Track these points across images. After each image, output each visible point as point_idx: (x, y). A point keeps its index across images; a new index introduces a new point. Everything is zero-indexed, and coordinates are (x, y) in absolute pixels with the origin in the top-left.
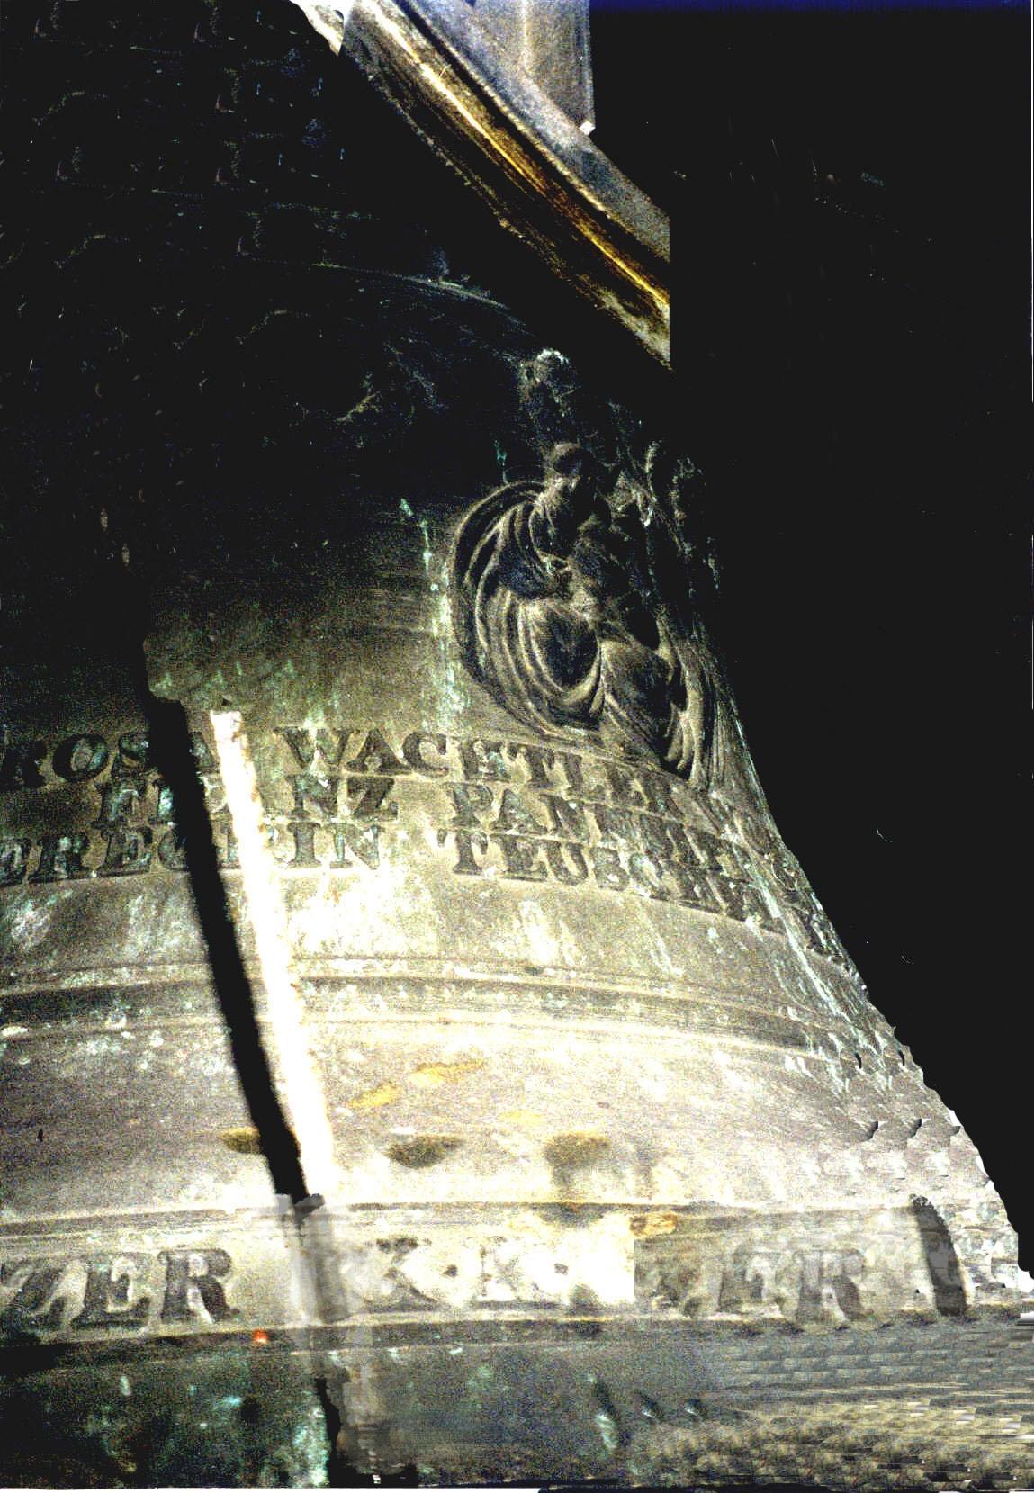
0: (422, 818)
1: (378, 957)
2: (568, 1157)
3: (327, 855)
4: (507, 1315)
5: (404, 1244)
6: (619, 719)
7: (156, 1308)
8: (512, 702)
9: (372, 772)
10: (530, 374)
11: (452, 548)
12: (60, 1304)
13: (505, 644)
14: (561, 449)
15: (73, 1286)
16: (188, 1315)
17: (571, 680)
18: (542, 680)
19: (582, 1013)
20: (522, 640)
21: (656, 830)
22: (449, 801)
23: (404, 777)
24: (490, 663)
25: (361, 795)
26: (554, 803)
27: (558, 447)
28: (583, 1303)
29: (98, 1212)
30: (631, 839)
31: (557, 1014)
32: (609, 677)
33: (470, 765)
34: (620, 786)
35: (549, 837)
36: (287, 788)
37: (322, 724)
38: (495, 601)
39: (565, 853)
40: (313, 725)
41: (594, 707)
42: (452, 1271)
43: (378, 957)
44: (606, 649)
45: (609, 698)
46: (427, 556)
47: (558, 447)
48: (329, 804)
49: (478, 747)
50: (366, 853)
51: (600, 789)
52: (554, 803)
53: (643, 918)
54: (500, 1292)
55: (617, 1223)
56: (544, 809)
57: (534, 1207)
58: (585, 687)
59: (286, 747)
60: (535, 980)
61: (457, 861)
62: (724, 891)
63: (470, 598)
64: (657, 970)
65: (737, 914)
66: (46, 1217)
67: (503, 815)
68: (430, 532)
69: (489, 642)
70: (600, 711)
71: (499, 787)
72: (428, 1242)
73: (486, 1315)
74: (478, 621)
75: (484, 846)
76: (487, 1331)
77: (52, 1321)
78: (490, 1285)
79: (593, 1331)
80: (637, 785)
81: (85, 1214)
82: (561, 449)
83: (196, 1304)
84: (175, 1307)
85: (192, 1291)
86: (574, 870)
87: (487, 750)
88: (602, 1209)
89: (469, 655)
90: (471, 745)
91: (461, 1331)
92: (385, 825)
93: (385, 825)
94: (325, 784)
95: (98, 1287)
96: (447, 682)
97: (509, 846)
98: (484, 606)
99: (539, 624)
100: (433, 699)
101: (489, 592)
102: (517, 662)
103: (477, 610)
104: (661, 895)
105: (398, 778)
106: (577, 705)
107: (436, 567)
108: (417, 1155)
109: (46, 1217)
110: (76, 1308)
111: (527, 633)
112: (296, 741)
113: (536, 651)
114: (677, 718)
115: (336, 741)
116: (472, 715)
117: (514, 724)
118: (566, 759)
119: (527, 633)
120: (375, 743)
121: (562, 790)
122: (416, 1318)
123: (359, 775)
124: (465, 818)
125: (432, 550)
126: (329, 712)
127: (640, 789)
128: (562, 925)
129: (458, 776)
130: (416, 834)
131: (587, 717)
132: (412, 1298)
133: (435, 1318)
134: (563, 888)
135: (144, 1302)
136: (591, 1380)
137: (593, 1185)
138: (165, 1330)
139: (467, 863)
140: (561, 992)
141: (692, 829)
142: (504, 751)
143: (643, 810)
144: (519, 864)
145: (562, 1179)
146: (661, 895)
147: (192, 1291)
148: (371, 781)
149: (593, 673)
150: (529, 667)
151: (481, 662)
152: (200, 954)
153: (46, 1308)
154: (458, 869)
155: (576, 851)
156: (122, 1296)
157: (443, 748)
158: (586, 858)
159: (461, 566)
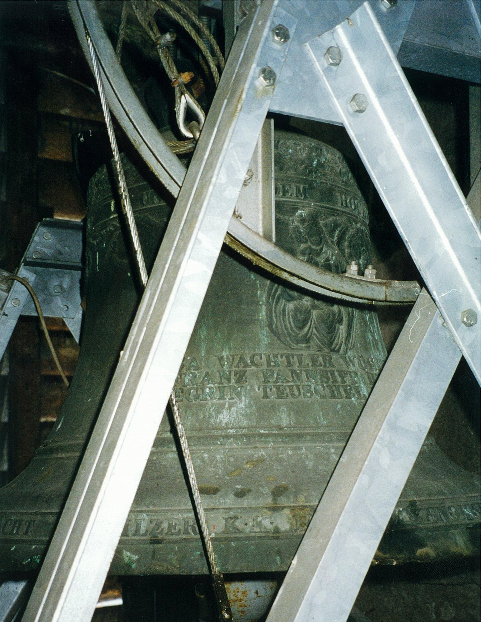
0: (254, 382)
1: (240, 428)
2: (279, 492)
3: (227, 397)
4: (258, 535)
5: (236, 518)
6: (317, 337)
7: (182, 532)
8: (283, 339)
9: (241, 368)
10: (293, 222)
11: (266, 288)
12: (162, 530)
13: (282, 319)
14: (303, 246)
15: (165, 525)
16: (189, 534)
17: (301, 328)
18: (292, 329)
19: (293, 442)
20: (287, 317)
21: (324, 374)
22: (262, 375)
23: (249, 369)
24: (276, 327)
25: (238, 376)
26: (293, 372)
27: (302, 245)
28: (277, 530)
29: (170, 508)
30: (315, 380)
31: (286, 442)
32: (315, 324)
33: (269, 365)
34: (314, 361)
35: (290, 384)
36: (218, 374)
37: (228, 353)
38: (279, 304)
39: (295, 390)
40: (225, 354)
41: (309, 336)
42: (246, 524)
43: (240, 428)
44: (314, 313)
45: (314, 330)
46: (259, 292)
47: (302, 245)
48: (229, 380)
49: (271, 357)
50: (238, 395)
51: (308, 364)
52: (293, 372)
53: (316, 406)
54: (257, 530)
55: (287, 512)
56: (290, 373)
57: (266, 508)
58: (306, 329)
59: (218, 361)
60: (282, 432)
61: (263, 395)
62: (345, 391)
63: (272, 306)
64: (318, 423)
65: (348, 397)
66: (159, 509)
67: (277, 379)
68: (260, 284)
69: (276, 319)
70: (311, 336)
71: (277, 368)
72: (241, 517)
73: (253, 534)
74: (274, 313)
75: (271, 389)
76: (253, 538)
77: (161, 533)
78: (255, 528)
79: (278, 538)
80: (321, 359)
81: (167, 508)
82: (303, 246)
83: (190, 531)
84: (186, 532)
85: (189, 528)
86: (296, 393)
87: (274, 357)
88: (283, 508)
89: (270, 326)
90: (269, 356)
91: (248, 538)
92: (244, 385)
93: (244, 385)
94: (228, 373)
95: (170, 526)
96: (264, 335)
97: (278, 388)
98: (275, 308)
99: (292, 310)
100: (259, 341)
101: (278, 302)
102: (285, 326)
103: (273, 309)
104: (324, 397)
105: (248, 369)
106: (302, 336)
107: (262, 296)
108: (240, 494)
109: (159, 509)
110: (166, 530)
111: (289, 315)
112: (221, 359)
113: (291, 320)
114: (338, 329)
115: (231, 358)
116: (271, 345)
117: (283, 346)
118: (297, 355)
119: (289, 315)
120: (242, 359)
121: (296, 367)
122: (238, 535)
123: (237, 369)
124: (266, 381)
125: (261, 290)
126: (230, 348)
127: (322, 361)
128: (292, 413)
129: (264, 367)
130: (252, 386)
131: (307, 340)
132: (238, 530)
133: (242, 535)
134: (293, 400)
135: (180, 530)
136: (276, 548)
137: (283, 500)
138: (184, 537)
139: (266, 396)
140: (289, 435)
141: (338, 371)
142: (279, 356)
143: (322, 367)
144: (280, 394)
145: (274, 500)
146: (324, 397)
147: (189, 528)
148: (241, 371)
149: (309, 324)
150: (289, 326)
151: (274, 327)
152: (159, 568)
153: (159, 531)
154: (263, 398)
155: (298, 387)
156: (175, 529)
157: (261, 358)
158: (301, 389)
159: (268, 297)
